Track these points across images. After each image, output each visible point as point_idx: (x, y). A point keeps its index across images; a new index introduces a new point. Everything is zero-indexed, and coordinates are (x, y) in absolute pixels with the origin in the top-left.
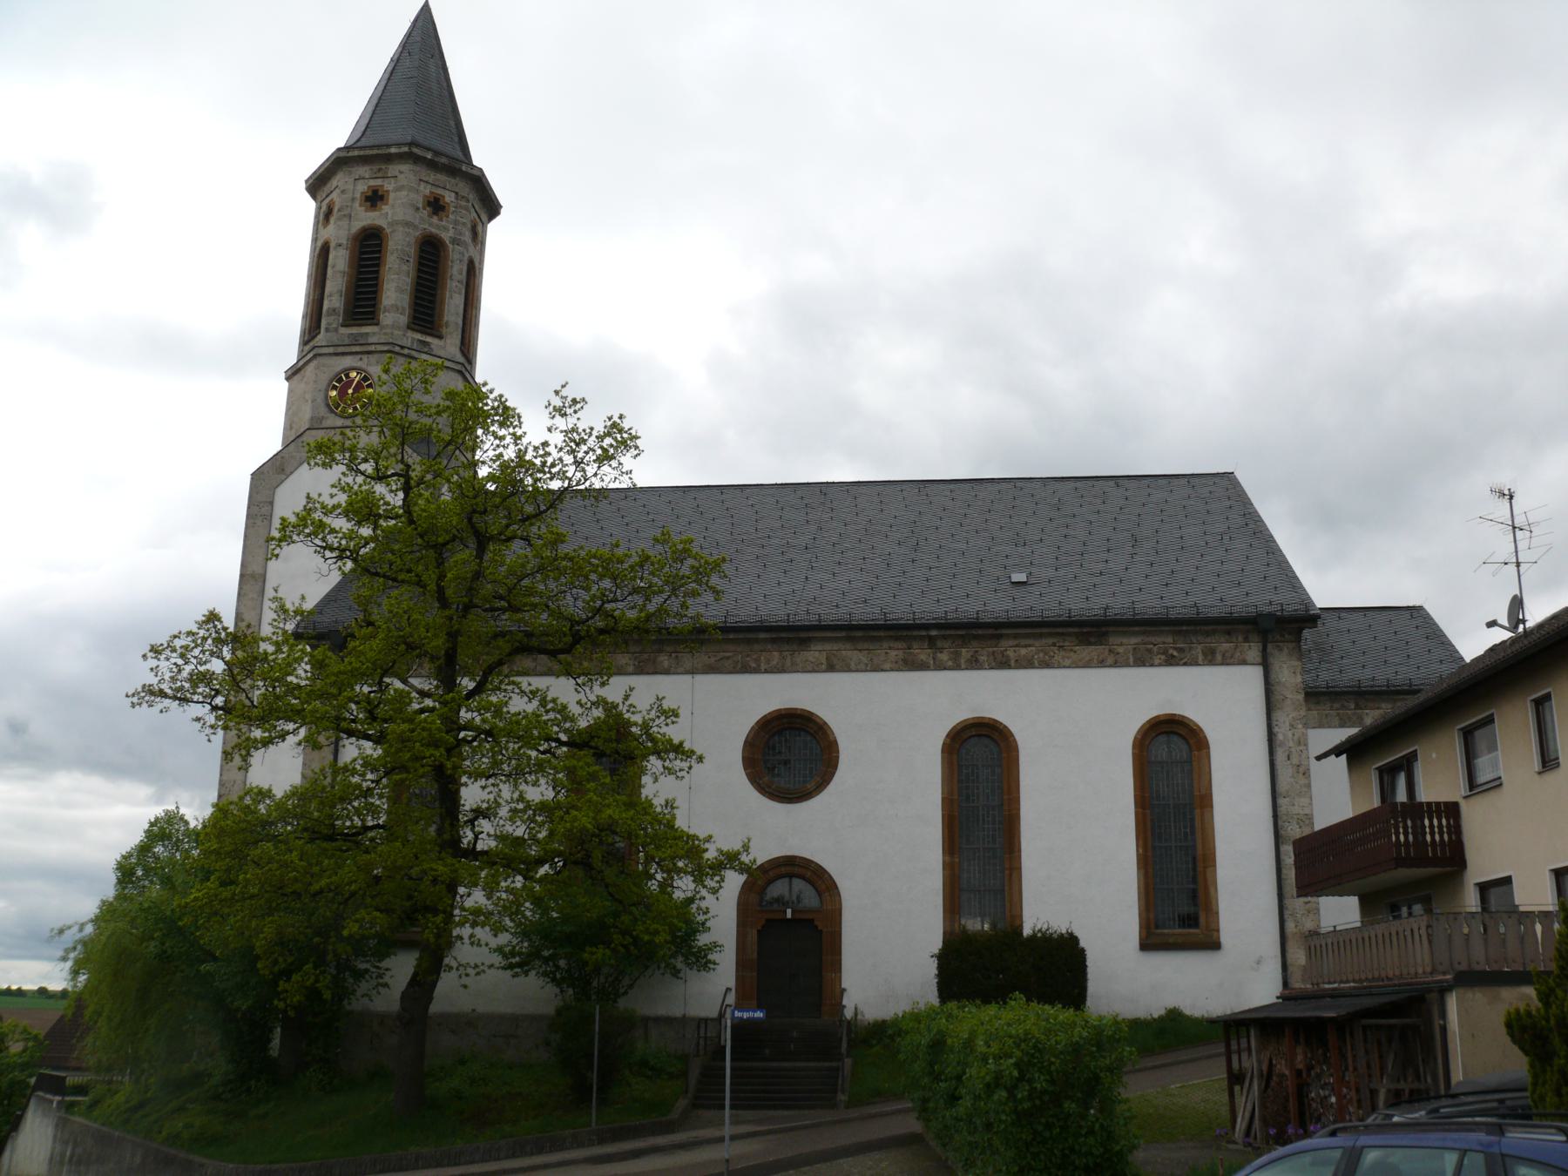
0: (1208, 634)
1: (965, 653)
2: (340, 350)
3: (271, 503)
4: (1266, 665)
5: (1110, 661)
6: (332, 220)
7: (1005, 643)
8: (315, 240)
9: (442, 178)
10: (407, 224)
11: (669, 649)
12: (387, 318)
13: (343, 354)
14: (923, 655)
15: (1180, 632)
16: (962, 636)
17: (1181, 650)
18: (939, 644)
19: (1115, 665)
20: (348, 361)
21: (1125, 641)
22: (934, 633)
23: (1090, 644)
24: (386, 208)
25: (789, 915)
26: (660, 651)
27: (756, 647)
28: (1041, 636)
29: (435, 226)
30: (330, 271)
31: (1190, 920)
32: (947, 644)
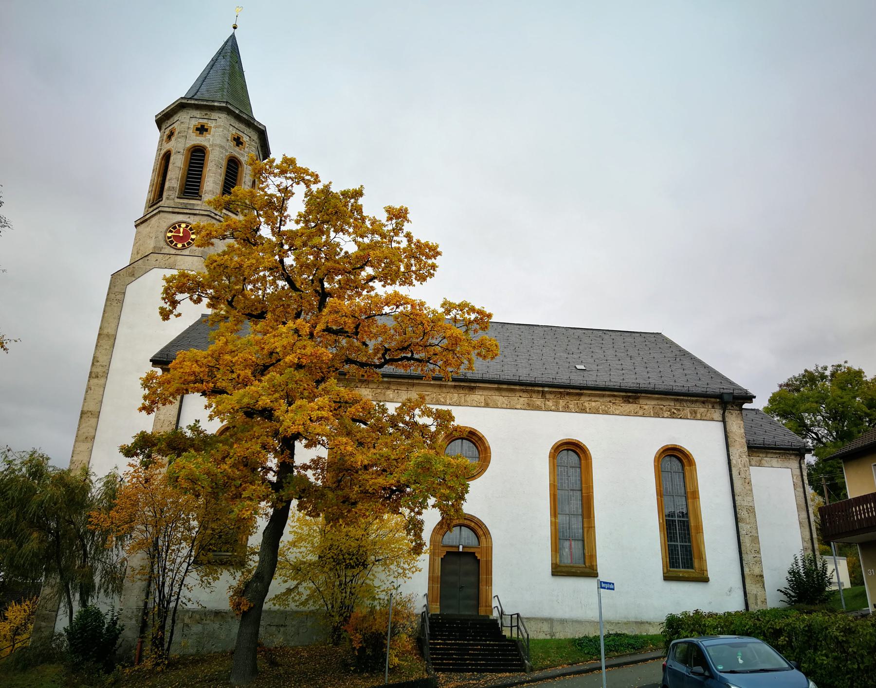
0: (692, 402)
1: (562, 403)
2: (177, 210)
3: (124, 293)
4: (724, 421)
5: (641, 413)
6: (173, 139)
7: (583, 398)
8: (160, 150)
9: (242, 127)
10: (222, 147)
11: (394, 388)
12: (207, 197)
13: (178, 213)
14: (539, 401)
15: (677, 400)
16: (561, 393)
17: (679, 410)
18: (548, 396)
19: (643, 416)
20: (180, 218)
21: (649, 402)
22: (546, 389)
23: (629, 402)
24: (208, 136)
25: (461, 550)
26: (388, 388)
27: (444, 390)
28: (603, 396)
29: (236, 152)
30: (170, 166)
31: (689, 564)
32: (552, 396)
